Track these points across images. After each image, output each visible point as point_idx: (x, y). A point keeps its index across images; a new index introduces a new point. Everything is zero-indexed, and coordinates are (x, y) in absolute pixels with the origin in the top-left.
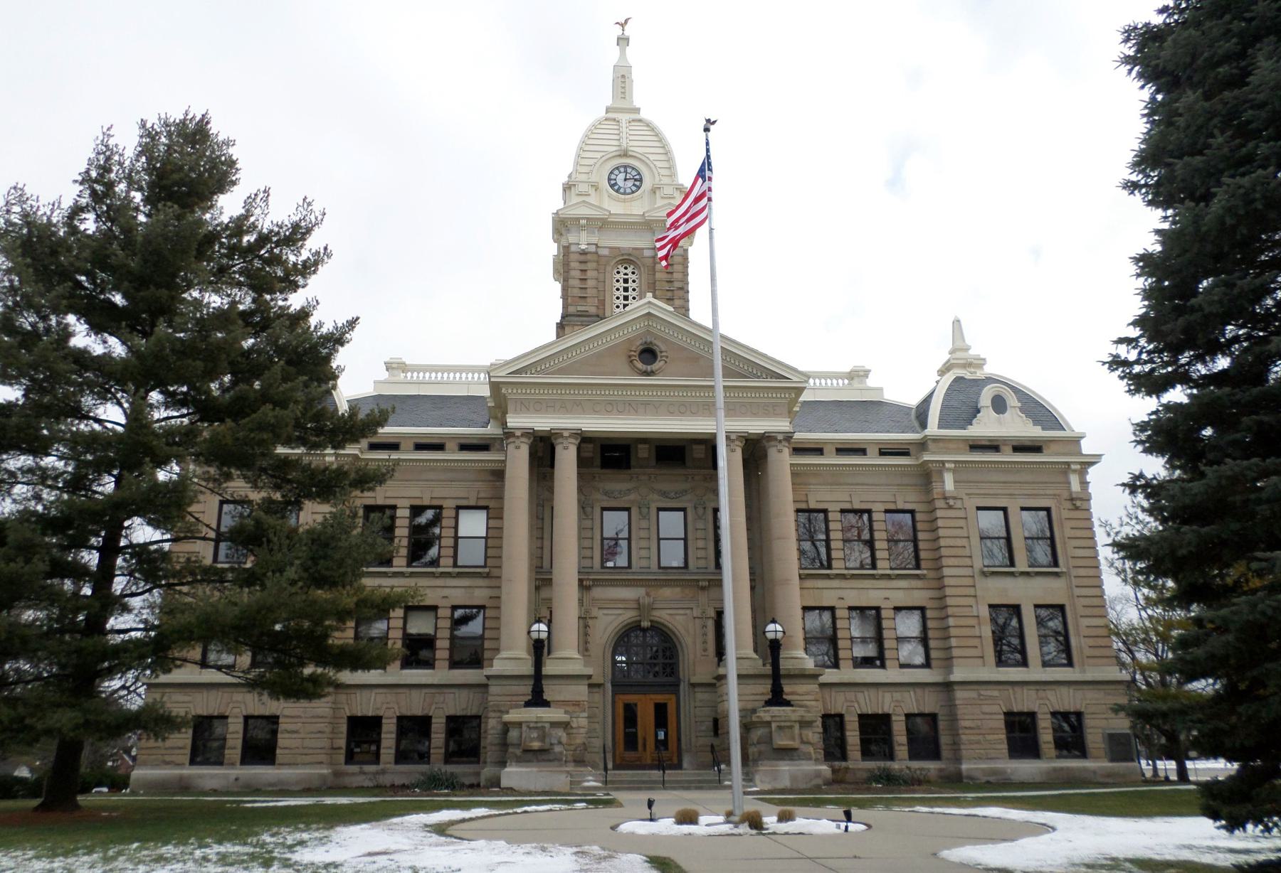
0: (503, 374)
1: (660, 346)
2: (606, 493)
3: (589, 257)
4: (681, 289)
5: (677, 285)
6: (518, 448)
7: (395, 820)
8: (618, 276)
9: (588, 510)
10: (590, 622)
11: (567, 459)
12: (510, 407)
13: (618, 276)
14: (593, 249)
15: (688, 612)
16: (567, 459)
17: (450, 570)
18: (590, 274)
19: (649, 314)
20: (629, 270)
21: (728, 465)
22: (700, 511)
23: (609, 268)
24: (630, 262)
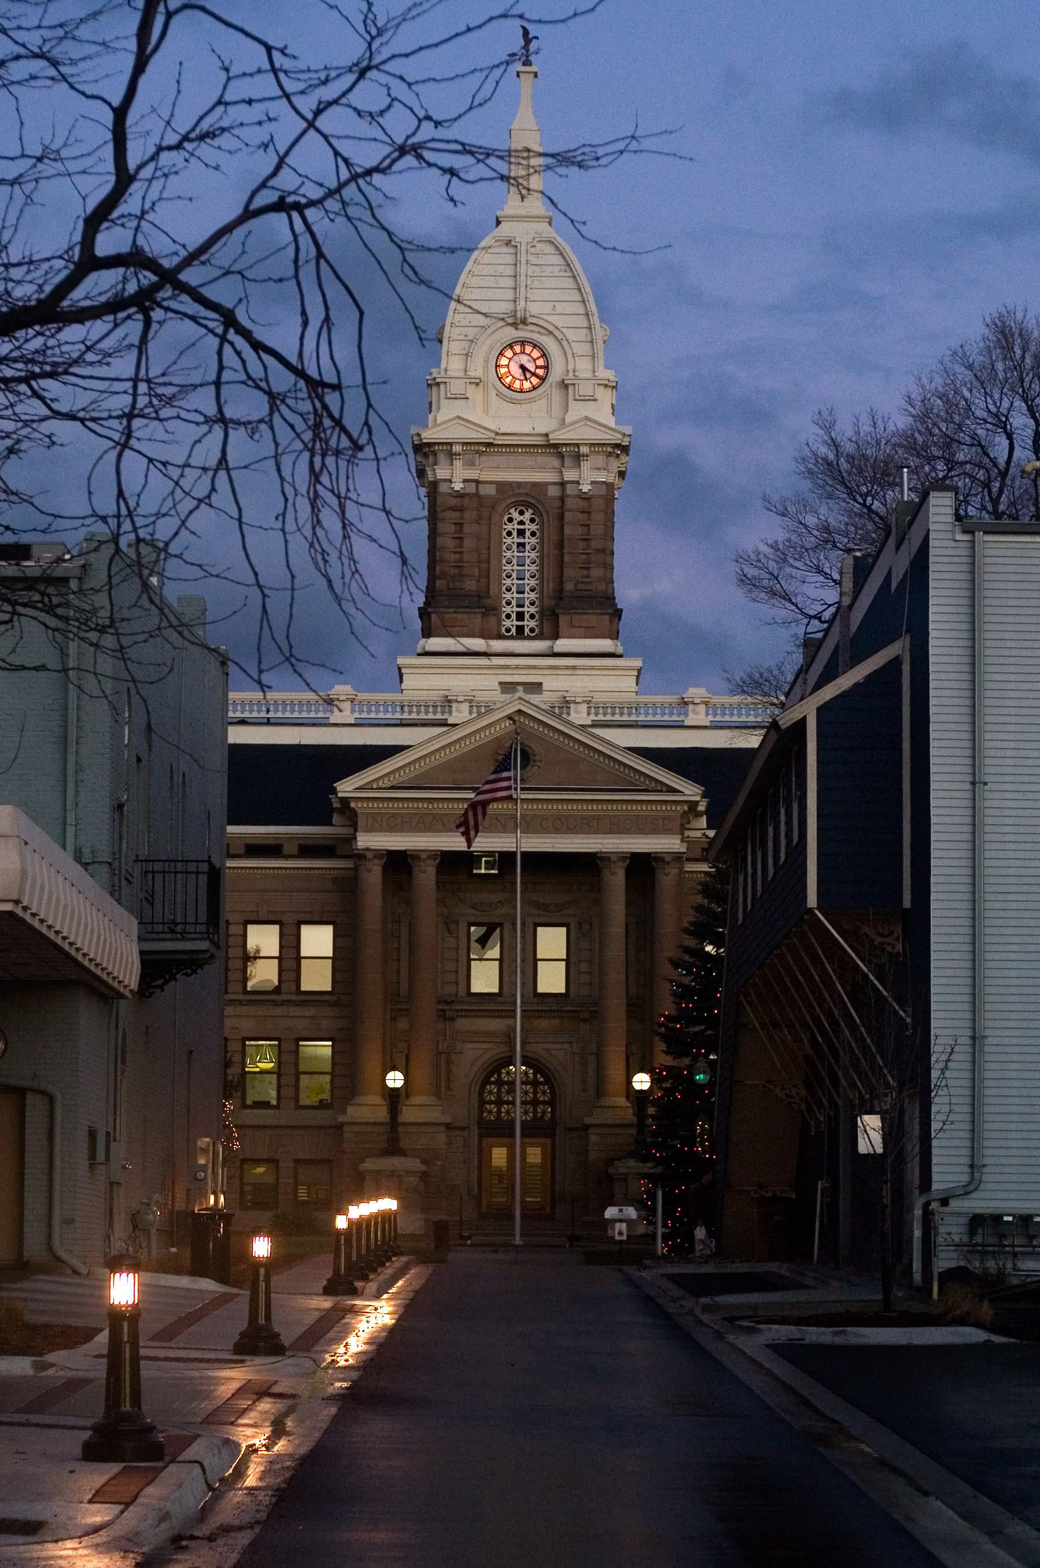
0: (350, 789)
1: (536, 748)
2: (474, 906)
3: (466, 502)
4: (602, 551)
5: (595, 544)
6: (370, 871)
7: (935, 1074)
8: (509, 527)
9: (453, 926)
10: (454, 1057)
11: (426, 877)
12: (361, 822)
13: (509, 527)
14: (471, 488)
15: (566, 1046)
16: (426, 877)
17: (293, 997)
18: (467, 529)
19: (520, 711)
20: (528, 515)
21: (617, 880)
22: (586, 927)
23: (495, 518)
24: (529, 505)
